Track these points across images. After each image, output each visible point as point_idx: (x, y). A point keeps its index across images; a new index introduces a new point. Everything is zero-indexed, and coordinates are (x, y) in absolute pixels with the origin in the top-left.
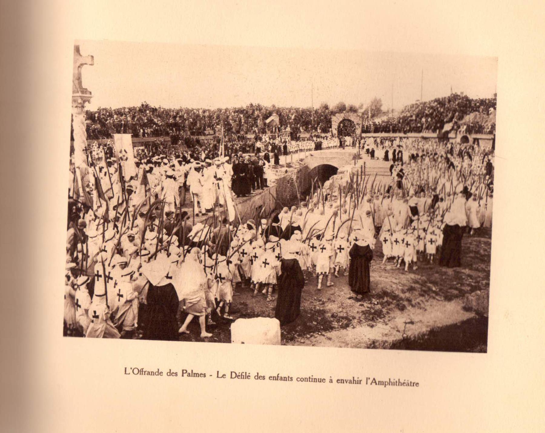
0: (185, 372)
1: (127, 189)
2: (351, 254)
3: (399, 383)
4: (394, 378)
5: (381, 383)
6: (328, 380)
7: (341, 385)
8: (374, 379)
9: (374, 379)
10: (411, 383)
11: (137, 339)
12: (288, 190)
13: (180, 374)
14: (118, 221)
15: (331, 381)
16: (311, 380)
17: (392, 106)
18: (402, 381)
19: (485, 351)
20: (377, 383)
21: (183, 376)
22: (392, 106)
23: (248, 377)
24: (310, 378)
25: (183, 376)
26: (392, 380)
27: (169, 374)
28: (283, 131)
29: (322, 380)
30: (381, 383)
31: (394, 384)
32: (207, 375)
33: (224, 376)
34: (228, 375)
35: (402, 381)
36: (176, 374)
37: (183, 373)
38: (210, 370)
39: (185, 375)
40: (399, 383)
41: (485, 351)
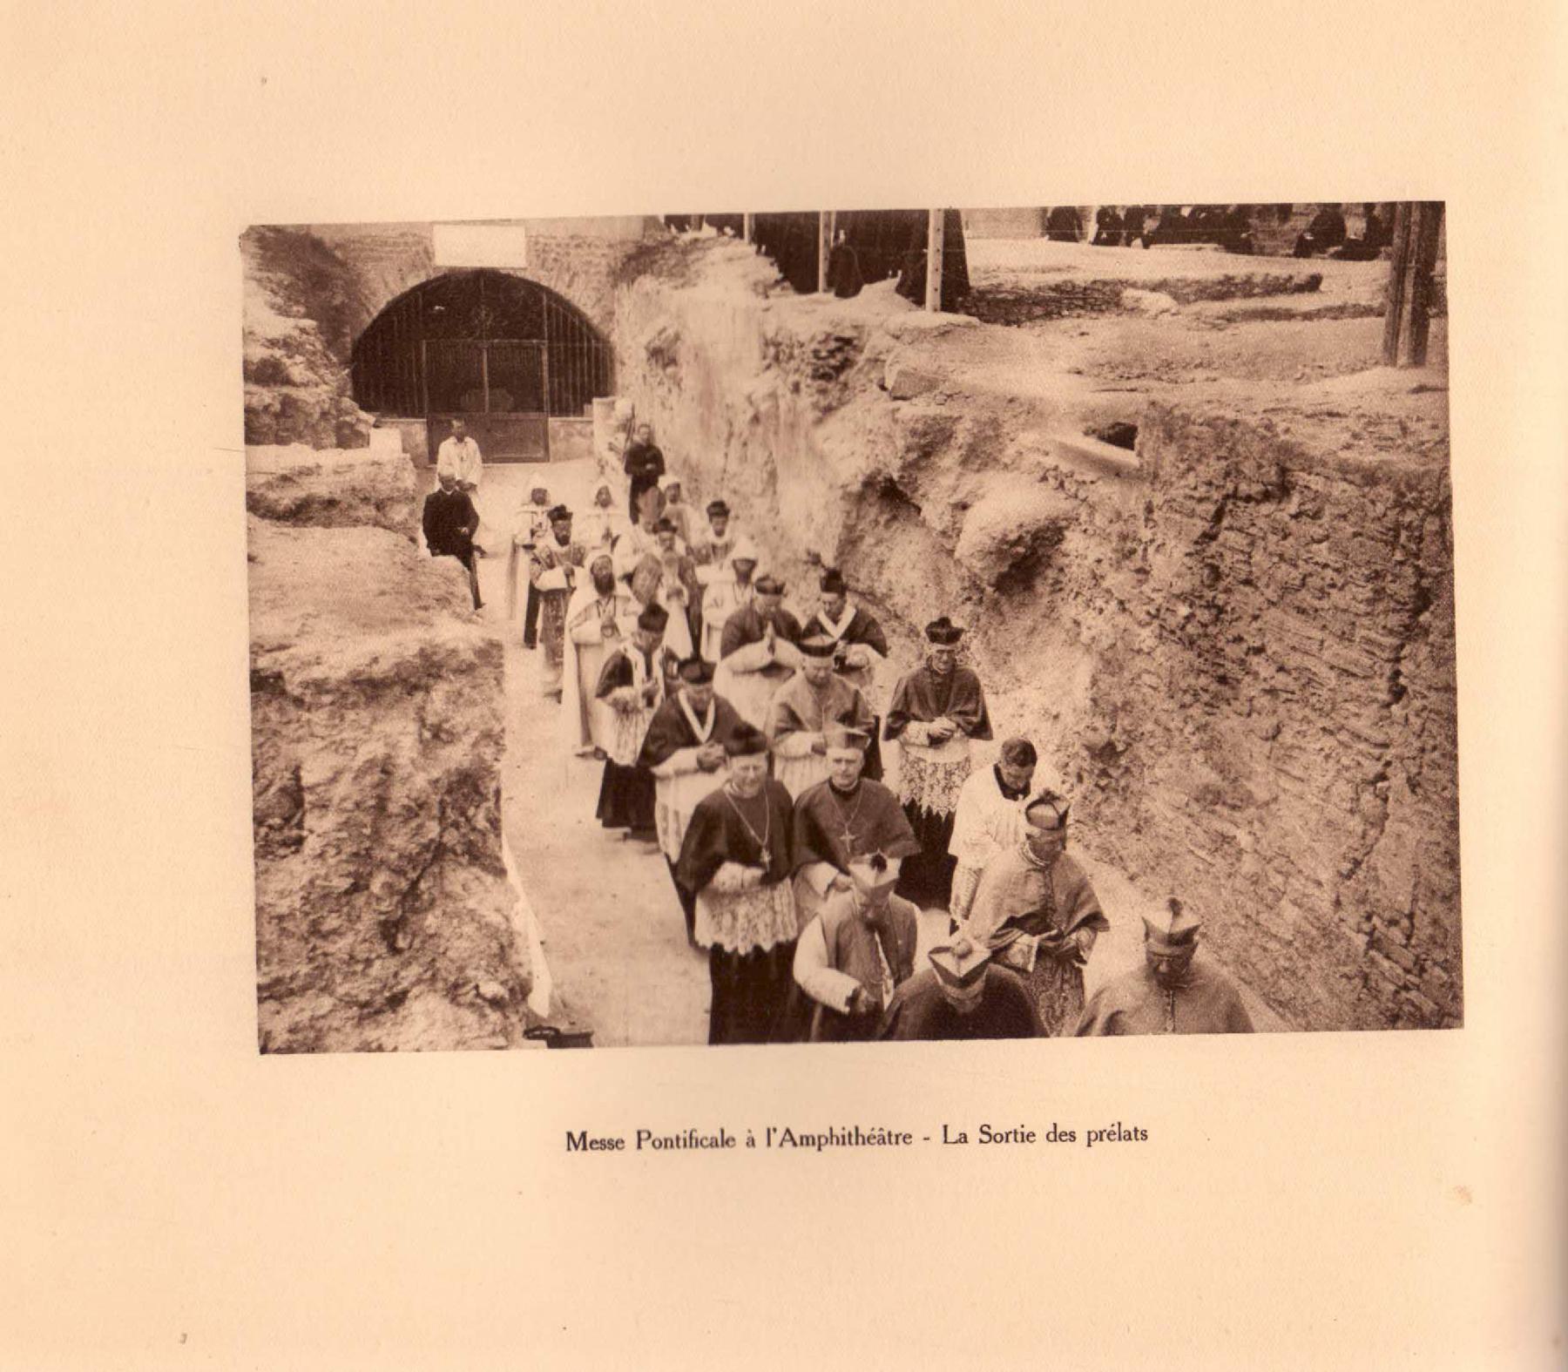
0: (644, 1135)
1: (539, 336)
5: (807, 1140)
6: (741, 1140)
7: (577, 1154)
8: (788, 1131)
10: (890, 1134)
12: (1439, 870)
13: (631, 1140)
14: (579, 563)
15: (751, 1142)
16: (1019, 1137)
17: (1368, 311)
21: (639, 1147)
22: (1368, 311)
23: (1028, 1137)
24: (885, 1133)
25: (639, 1147)
26: (838, 1132)
27: (1052, 1136)
30: (807, 1140)
31: (843, 1141)
33: (964, 1139)
34: (974, 1136)
35: (865, 1131)
36: (1072, 1136)
37: (640, 1140)
38: (921, 1123)
39: (646, 1145)
40: (855, 1138)
41: (1443, 204)
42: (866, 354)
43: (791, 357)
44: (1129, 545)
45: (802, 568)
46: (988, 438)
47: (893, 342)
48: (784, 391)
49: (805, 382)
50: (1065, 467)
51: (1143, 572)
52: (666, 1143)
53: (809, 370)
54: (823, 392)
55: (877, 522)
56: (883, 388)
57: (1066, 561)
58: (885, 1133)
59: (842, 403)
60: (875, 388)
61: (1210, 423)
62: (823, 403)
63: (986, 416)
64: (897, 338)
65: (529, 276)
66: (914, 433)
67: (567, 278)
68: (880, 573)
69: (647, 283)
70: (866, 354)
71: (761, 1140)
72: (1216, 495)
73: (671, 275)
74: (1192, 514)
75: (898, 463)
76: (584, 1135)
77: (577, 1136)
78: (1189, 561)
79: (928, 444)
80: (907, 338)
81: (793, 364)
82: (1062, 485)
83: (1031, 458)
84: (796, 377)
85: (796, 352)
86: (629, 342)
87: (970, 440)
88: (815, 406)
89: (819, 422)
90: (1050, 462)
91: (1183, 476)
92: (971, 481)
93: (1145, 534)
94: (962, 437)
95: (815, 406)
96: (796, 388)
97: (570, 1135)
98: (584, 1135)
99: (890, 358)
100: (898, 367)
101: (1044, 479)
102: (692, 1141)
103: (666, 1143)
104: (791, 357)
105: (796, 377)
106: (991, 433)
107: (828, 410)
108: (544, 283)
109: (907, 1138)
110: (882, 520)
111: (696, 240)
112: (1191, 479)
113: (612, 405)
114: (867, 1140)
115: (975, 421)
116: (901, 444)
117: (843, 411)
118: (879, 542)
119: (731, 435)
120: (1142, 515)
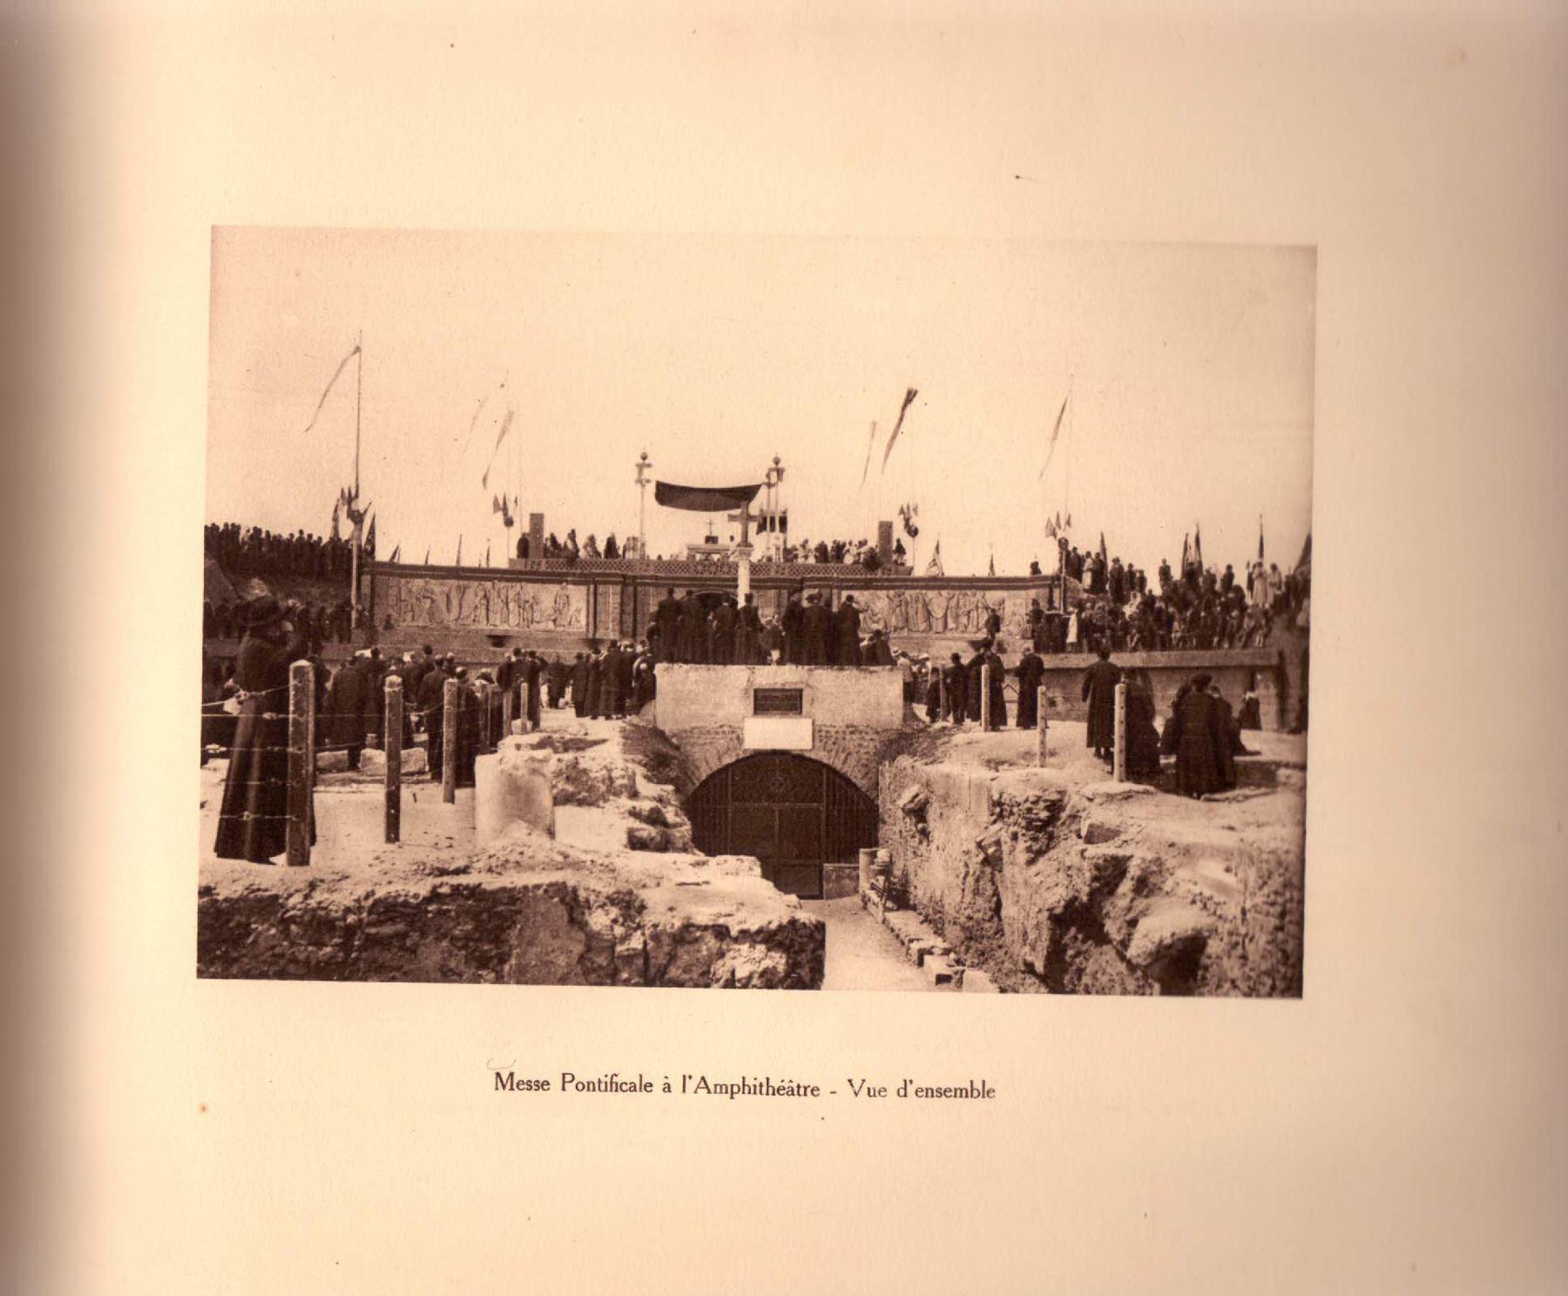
0: (568, 1078)
2: (711, 852)
3: (767, 1088)
4: (755, 1074)
8: (703, 1078)
9: (703, 1078)
11: (662, 985)
13: (556, 1083)
15: (667, 1088)
18: (775, 1083)
19: (201, 974)
20: (712, 1088)
24: (794, 1085)
26: (750, 1082)
28: (1224, 928)
29: (542, 1085)
31: (756, 1090)
32: (824, 1091)
35: (775, 1083)
38: (828, 1075)
39: (570, 1087)
41: (201, 974)
42: (1068, 812)
43: (1011, 813)
44: (1234, 938)
45: (1020, 976)
46: (1153, 873)
47: (1087, 803)
48: (1005, 837)
49: (1021, 832)
50: (1207, 893)
51: (1244, 957)
52: (589, 1086)
53: (1023, 823)
54: (1035, 839)
55: (1075, 938)
56: (1079, 836)
57: (1208, 962)
58: (794, 1085)
59: (1048, 848)
60: (1074, 836)
61: (1272, 852)
62: (1036, 847)
63: (1150, 856)
64: (1090, 800)
65: (813, 756)
66: (1097, 868)
67: (843, 756)
68: (1079, 979)
69: (904, 761)
70: (1068, 812)
71: (676, 1085)
72: (1280, 900)
73: (924, 755)
74: (1268, 914)
75: (1086, 889)
76: (511, 1075)
77: (505, 1077)
78: (1269, 947)
79: (1110, 874)
80: (1098, 800)
81: (1012, 819)
82: (1205, 906)
83: (1181, 890)
84: (1015, 829)
85: (1015, 810)
86: (889, 806)
87: (1138, 873)
88: (1029, 849)
89: (1031, 862)
90: (1197, 890)
91: (1261, 888)
92: (1141, 904)
93: (1243, 930)
94: (1134, 870)
95: (1029, 849)
96: (1015, 837)
97: (498, 1075)
98: (511, 1075)
99: (1083, 814)
100: (1088, 822)
101: (1194, 902)
102: (613, 1085)
103: (589, 1086)
104: (1011, 813)
105: (1015, 829)
106: (1154, 868)
107: (1040, 853)
108: (825, 761)
109: (815, 1091)
110: (1080, 936)
111: (944, 728)
112: (1266, 890)
113: (873, 855)
114: (778, 1091)
115: (1144, 860)
116: (1088, 875)
117: (1052, 853)
118: (1078, 954)
119: (967, 874)
120: (1239, 916)
